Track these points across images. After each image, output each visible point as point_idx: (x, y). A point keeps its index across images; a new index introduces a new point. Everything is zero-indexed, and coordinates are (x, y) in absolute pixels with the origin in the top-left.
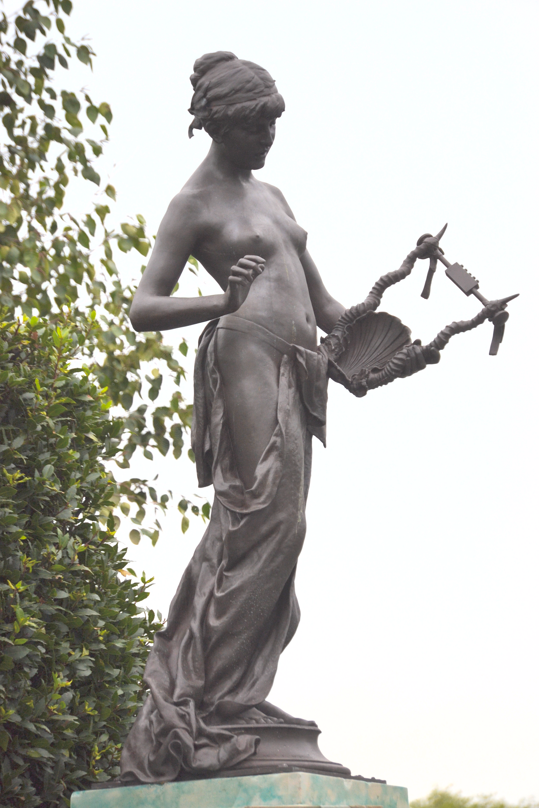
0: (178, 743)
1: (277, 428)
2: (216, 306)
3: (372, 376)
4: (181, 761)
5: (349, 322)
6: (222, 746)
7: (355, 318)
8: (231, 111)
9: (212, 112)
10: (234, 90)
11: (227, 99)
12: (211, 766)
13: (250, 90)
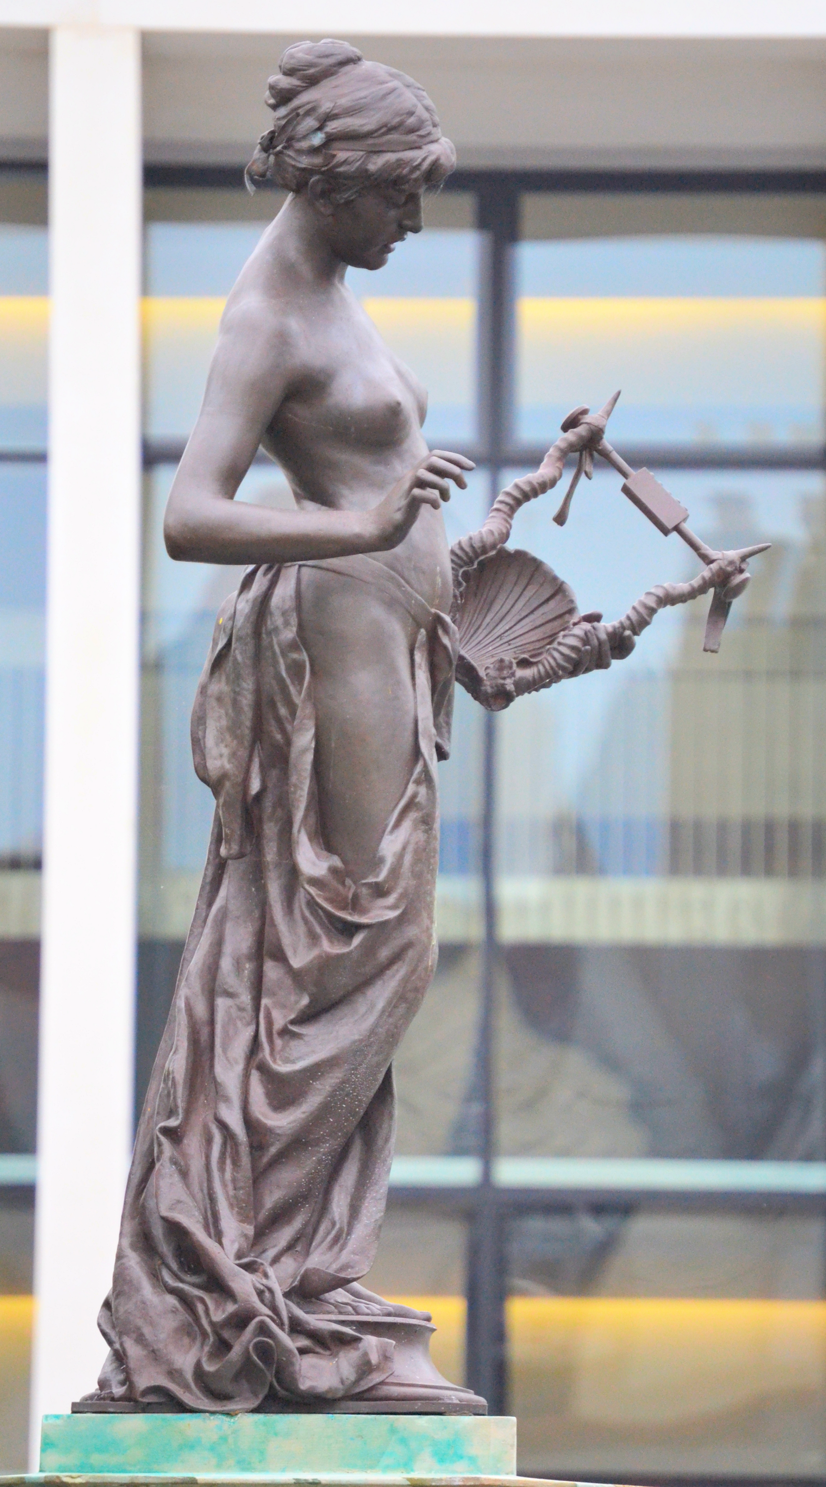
0: (267, 1343)
1: (419, 768)
2: (358, 536)
3: (521, 673)
4: (270, 1377)
5: (466, 564)
6: (341, 1354)
7: (477, 557)
8: (376, 164)
9: (335, 161)
10: (386, 126)
11: (370, 141)
12: (330, 1390)
13: (412, 131)
